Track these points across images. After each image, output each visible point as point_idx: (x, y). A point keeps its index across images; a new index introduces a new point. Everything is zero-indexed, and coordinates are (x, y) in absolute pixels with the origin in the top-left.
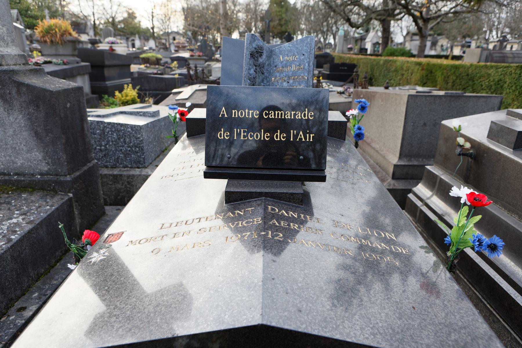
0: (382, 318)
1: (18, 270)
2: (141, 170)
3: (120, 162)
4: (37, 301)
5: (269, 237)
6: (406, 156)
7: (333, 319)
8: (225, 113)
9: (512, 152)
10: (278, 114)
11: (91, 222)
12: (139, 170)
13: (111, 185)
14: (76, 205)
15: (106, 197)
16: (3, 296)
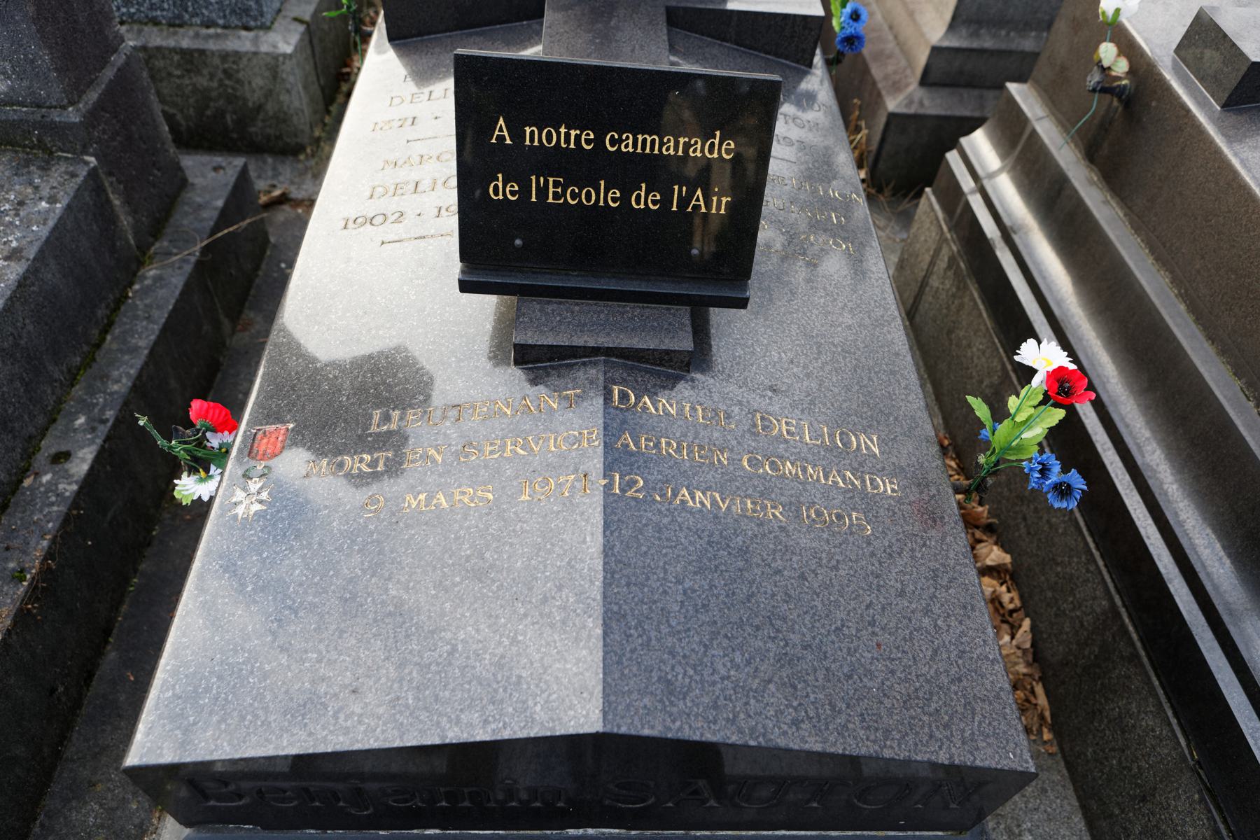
0: (817, 681)
1: (25, 375)
2: (257, 38)
3: (190, 9)
4: (89, 436)
5: (615, 494)
6: (968, 22)
7: (731, 700)
8: (506, 133)
9: (1217, 115)
10: (644, 141)
11: (158, 215)
12: (251, 34)
13: (179, 77)
14: (111, 183)
15: (172, 111)
16: (10, 436)
